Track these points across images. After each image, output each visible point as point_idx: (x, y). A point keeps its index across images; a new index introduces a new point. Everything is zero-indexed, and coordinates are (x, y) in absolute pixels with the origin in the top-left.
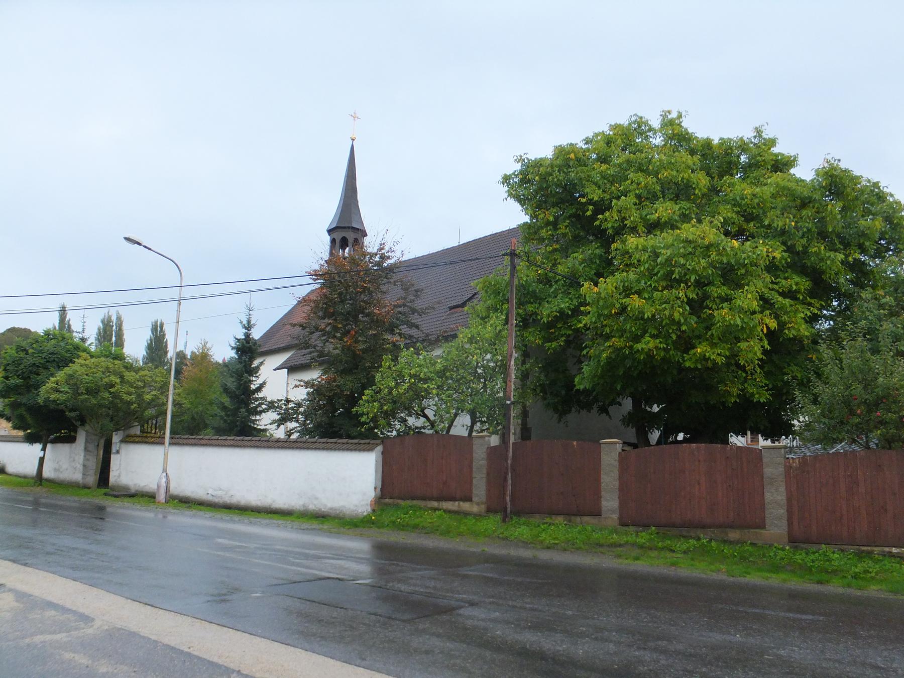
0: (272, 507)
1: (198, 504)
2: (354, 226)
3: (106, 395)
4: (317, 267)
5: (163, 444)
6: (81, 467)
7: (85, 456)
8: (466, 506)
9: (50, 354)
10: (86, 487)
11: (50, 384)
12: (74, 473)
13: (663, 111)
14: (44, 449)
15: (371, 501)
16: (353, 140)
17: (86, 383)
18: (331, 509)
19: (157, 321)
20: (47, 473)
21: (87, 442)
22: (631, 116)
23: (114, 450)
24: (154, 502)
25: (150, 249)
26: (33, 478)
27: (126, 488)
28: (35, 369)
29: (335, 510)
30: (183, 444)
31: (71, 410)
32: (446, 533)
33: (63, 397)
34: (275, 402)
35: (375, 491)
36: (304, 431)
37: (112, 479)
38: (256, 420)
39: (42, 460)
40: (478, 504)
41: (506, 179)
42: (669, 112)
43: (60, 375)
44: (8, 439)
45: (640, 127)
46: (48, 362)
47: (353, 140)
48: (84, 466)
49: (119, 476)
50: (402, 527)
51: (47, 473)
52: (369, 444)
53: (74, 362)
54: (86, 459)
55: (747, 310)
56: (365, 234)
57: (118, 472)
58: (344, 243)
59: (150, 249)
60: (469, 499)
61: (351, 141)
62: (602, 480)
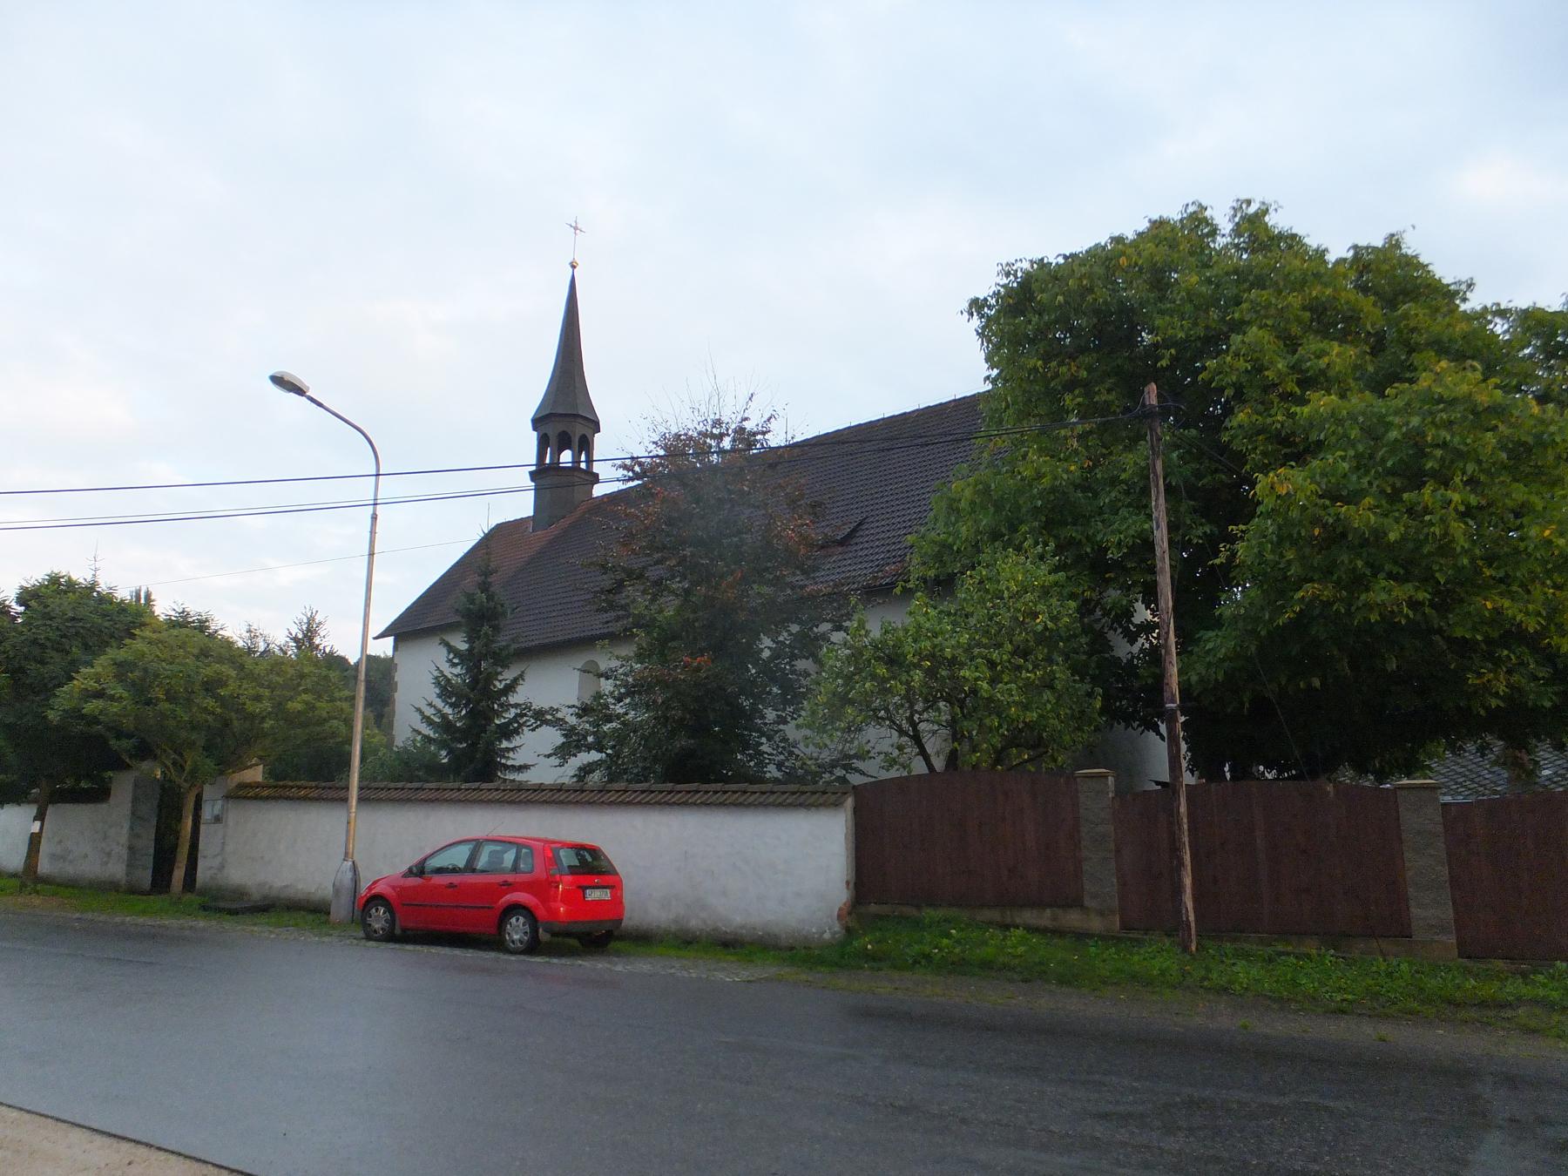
0: (282, 896)
1: (9, 876)
2: (581, 413)
3: (210, 703)
4: (640, 452)
5: (345, 800)
6: (124, 853)
7: (132, 828)
8: (1073, 919)
9: (67, 620)
10: (133, 890)
11: (84, 679)
12: (107, 863)
13: (1238, 200)
14: (40, 817)
15: (840, 909)
16: (574, 267)
17: (167, 677)
18: (743, 927)
19: (140, 590)
20: (44, 866)
21: (135, 800)
22: (1187, 205)
23: (207, 813)
24: (327, 922)
25: (320, 405)
26: (14, 875)
27: (239, 893)
28: (36, 651)
29: (754, 929)
30: (379, 800)
31: (120, 735)
32: (1068, 980)
33: (115, 708)
34: (546, 712)
35: (848, 888)
36: (614, 769)
37: (203, 874)
38: (508, 750)
39: (35, 841)
40: (1101, 913)
41: (977, 305)
42: (1249, 202)
43: (102, 664)
44: (547, 796)
45: (1198, 221)
46: (64, 636)
47: (574, 267)
48: (131, 848)
49: (222, 867)
50: (958, 967)
51: (44, 866)
52: (403, 789)
53: (133, 636)
54: (134, 835)
55: (270, 668)
56: (596, 427)
57: (219, 859)
58: (564, 443)
59: (320, 405)
60: (1076, 903)
61: (571, 270)
62: (1407, 864)
